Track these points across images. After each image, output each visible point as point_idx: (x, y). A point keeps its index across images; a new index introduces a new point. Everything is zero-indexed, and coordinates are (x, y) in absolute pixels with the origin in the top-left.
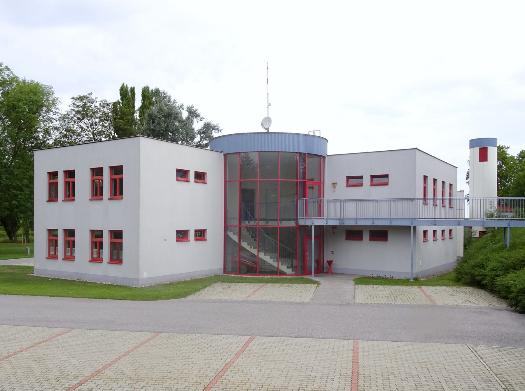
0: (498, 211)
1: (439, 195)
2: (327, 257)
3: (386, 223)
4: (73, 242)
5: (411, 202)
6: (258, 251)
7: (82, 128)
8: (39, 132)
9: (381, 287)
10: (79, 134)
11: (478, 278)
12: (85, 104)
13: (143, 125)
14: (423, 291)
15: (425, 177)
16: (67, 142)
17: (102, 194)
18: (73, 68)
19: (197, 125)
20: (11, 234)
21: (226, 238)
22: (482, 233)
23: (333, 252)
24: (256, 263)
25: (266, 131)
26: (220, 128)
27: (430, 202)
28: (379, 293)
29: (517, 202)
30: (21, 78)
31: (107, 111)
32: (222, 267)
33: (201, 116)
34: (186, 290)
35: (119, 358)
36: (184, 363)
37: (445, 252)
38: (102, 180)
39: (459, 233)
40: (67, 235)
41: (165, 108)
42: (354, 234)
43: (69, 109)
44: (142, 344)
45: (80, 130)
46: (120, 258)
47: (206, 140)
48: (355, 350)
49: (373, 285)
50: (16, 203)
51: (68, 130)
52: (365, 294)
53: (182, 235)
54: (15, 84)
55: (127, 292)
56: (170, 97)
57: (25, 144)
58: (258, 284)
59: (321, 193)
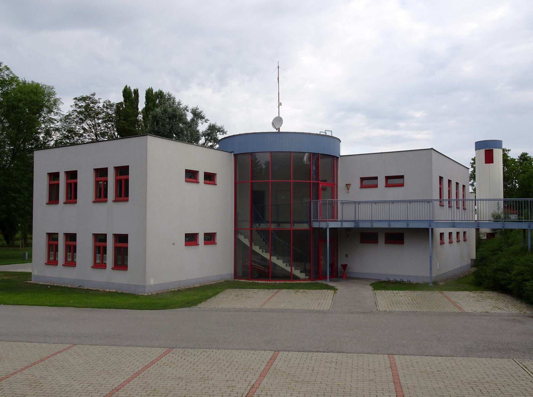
0: (505, 213)
1: (454, 196)
2: (342, 261)
3: (403, 225)
4: (75, 247)
5: (409, 204)
6: (271, 255)
7: (84, 129)
8: (40, 133)
9: (402, 293)
10: (82, 135)
11: (503, 283)
12: (88, 105)
13: (146, 126)
14: (446, 297)
15: (441, 178)
16: (69, 143)
17: (106, 196)
18: (75, 67)
19: (202, 127)
20: (9, 238)
21: (237, 243)
22: (491, 236)
23: (347, 255)
24: (268, 267)
25: (277, 131)
26: (225, 131)
27: (446, 203)
28: (401, 299)
29: (528, 203)
30: (21, 79)
31: (110, 112)
32: (231, 270)
33: (206, 118)
34: (196, 297)
35: (128, 381)
36: (203, 386)
37: (457, 255)
38: (107, 181)
39: (472, 234)
40: (68, 239)
41: (170, 110)
42: (368, 236)
43: (71, 109)
44: (153, 363)
45: (82, 131)
46: (125, 263)
47: (211, 142)
48: (393, 367)
49: (393, 290)
50: (14, 206)
51: (69, 131)
52: (386, 299)
53: (191, 239)
54: (15, 84)
55: (134, 301)
56: (174, 98)
57: (24, 146)
58: (272, 290)
59: (334, 194)
